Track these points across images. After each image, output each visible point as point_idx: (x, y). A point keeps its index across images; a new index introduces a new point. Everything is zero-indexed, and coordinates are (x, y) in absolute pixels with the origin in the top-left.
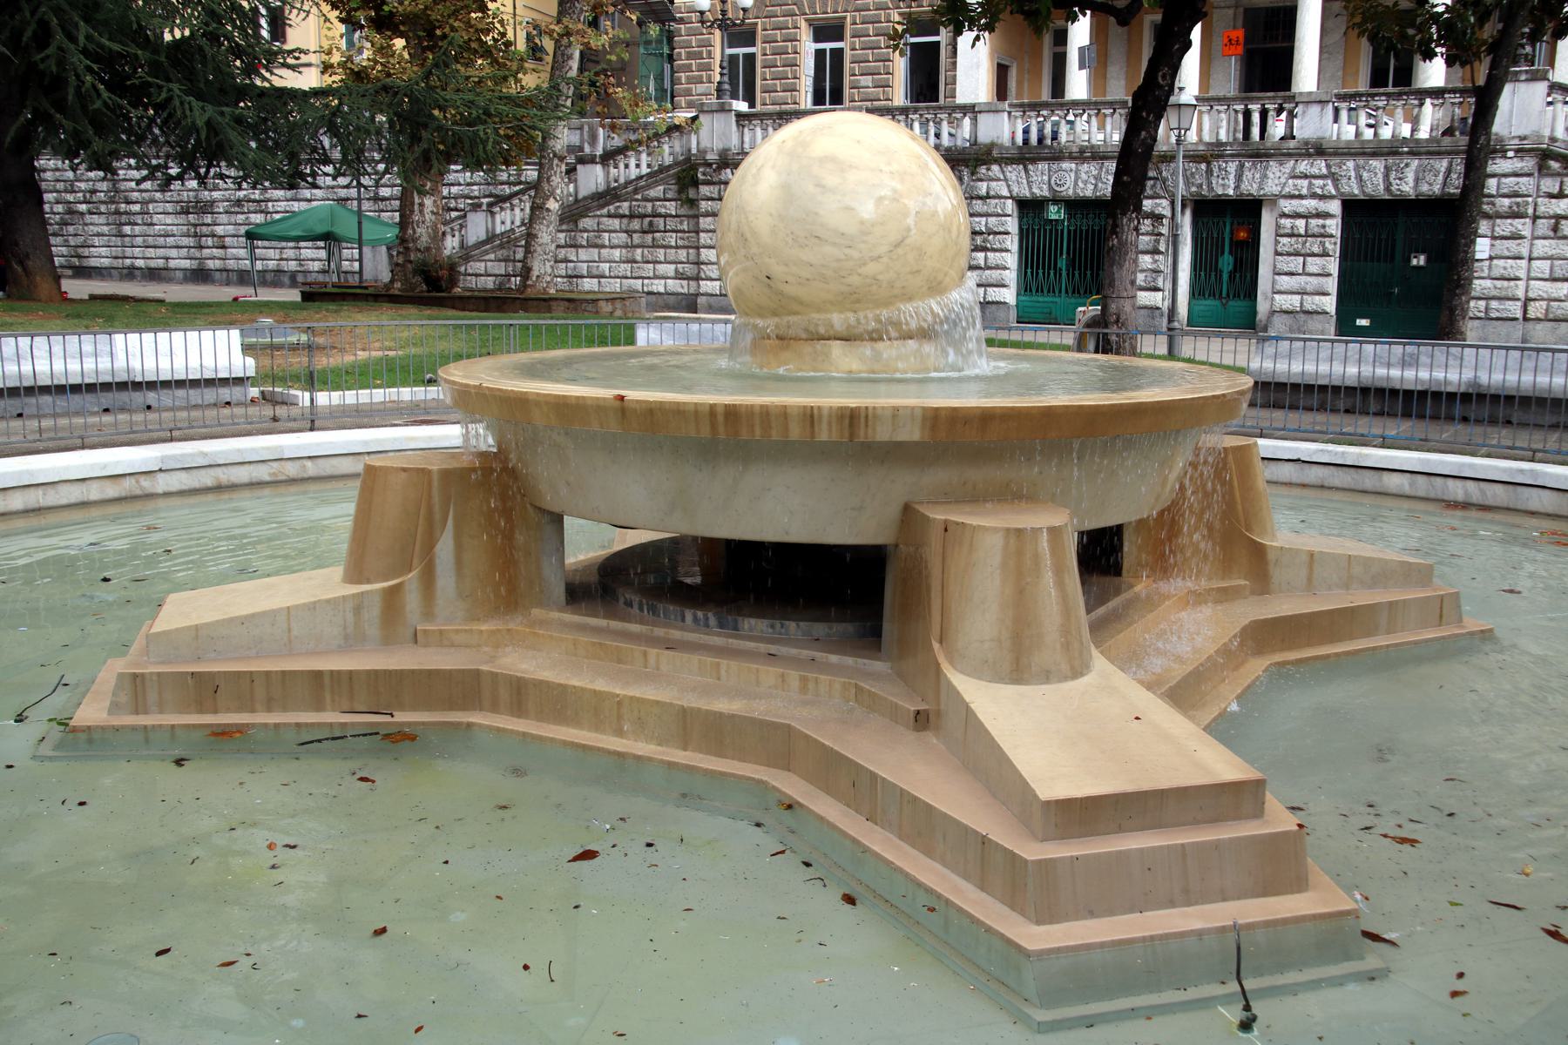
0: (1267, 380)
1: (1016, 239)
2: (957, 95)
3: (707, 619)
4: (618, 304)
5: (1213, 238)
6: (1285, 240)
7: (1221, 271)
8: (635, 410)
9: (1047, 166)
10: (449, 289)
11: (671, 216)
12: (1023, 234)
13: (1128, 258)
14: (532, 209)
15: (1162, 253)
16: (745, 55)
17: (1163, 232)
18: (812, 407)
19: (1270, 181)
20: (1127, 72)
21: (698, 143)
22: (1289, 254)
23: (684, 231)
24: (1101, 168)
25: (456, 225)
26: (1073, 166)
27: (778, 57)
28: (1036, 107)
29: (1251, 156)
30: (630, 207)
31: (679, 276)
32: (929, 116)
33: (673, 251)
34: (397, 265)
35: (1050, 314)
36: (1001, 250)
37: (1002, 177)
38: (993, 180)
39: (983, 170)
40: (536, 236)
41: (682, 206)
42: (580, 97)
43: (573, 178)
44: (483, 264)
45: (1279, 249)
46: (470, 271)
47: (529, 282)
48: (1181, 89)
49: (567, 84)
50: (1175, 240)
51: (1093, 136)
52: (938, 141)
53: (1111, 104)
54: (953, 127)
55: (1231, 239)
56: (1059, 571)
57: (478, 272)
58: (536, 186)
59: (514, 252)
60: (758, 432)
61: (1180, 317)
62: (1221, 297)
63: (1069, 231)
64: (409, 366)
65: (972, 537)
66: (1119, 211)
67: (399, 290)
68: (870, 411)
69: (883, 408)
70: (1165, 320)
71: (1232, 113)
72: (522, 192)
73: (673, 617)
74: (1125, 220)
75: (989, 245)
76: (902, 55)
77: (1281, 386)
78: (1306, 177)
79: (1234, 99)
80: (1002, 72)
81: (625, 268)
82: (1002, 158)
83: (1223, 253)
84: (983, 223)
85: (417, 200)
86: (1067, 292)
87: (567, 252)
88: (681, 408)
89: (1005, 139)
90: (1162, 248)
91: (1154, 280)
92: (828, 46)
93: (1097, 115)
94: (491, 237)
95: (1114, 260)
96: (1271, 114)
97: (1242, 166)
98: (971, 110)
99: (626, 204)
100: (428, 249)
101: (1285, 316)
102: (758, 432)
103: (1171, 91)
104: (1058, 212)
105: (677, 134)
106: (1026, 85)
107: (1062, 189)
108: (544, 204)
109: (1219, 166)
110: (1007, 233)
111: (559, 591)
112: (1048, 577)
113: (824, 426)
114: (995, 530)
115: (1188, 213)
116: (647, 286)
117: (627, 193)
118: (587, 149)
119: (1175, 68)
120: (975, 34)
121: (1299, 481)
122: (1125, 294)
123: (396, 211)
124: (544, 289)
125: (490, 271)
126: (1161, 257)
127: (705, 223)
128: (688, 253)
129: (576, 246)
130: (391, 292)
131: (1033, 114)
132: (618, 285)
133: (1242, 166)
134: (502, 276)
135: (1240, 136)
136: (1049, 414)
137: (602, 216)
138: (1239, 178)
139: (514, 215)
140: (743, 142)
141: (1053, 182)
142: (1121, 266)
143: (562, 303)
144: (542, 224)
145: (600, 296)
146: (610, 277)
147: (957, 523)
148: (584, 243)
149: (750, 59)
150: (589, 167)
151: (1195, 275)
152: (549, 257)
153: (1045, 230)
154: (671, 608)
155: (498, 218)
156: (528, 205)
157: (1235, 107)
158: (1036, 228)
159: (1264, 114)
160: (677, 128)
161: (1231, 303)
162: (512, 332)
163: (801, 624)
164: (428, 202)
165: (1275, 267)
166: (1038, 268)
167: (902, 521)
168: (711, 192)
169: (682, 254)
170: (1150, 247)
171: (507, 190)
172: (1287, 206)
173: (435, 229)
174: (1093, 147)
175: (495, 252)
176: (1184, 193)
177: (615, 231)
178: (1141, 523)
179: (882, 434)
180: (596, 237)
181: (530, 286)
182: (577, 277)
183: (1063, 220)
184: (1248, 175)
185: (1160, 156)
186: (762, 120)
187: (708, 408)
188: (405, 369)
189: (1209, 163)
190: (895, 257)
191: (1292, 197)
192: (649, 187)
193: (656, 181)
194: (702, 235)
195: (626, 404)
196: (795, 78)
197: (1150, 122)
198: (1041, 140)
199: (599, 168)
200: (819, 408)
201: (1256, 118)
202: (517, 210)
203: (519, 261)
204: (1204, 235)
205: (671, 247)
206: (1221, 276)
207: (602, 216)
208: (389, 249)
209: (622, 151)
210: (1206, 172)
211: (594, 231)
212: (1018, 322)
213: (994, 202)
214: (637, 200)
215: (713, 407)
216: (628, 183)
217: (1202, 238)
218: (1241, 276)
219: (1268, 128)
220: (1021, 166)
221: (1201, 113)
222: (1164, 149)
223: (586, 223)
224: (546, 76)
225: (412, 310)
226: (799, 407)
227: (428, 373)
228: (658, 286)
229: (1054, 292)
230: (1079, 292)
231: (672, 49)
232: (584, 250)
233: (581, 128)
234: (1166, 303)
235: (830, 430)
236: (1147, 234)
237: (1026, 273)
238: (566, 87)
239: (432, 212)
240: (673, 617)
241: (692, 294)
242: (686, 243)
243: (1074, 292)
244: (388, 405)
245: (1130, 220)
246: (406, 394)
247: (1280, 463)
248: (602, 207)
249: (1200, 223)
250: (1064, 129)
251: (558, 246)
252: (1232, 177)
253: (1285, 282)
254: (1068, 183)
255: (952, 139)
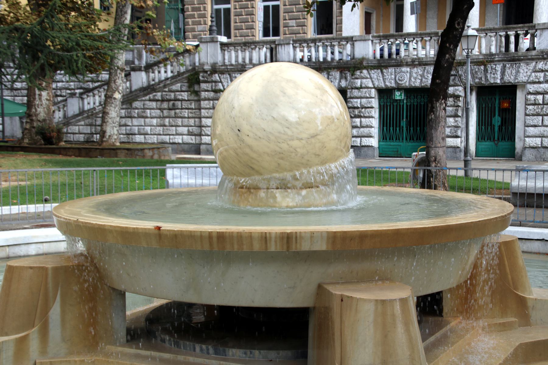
0: (522, 192)
1: (377, 111)
2: (343, 29)
3: (208, 349)
4: (156, 151)
5: (488, 107)
6: (531, 107)
7: (494, 126)
8: (167, 235)
9: (393, 70)
10: (57, 144)
11: (185, 100)
12: (382, 108)
13: (440, 125)
14: (105, 96)
15: (460, 116)
16: (225, 9)
17: (460, 105)
18: (266, 233)
19: (521, 74)
20: (438, 14)
21: (199, 60)
22: (533, 115)
23: (192, 109)
24: (424, 70)
25: (61, 105)
26: (408, 69)
27: (243, 10)
28: (387, 37)
29: (510, 61)
30: (162, 95)
31: (190, 134)
32: (327, 44)
33: (186, 120)
34: (26, 129)
35: (397, 151)
36: (369, 117)
37: (369, 76)
38: (363, 78)
39: (358, 73)
40: (108, 113)
41: (191, 95)
42: (132, 36)
43: (129, 79)
44: (77, 127)
45: (528, 113)
46: (70, 131)
47: (105, 139)
48: (468, 27)
49: (124, 28)
50: (467, 110)
51: (419, 52)
52: (333, 56)
53: (429, 34)
54: (341, 48)
55: (499, 108)
56: (407, 324)
57: (74, 132)
58: (108, 83)
59: (96, 121)
60: (236, 247)
61: (471, 152)
62: (494, 140)
63: (407, 106)
64: (34, 191)
65: (357, 305)
66: (434, 100)
67: (27, 144)
68: (298, 235)
69: (305, 232)
70: (462, 154)
71: (499, 37)
72: (100, 87)
73: (188, 348)
74: (438, 104)
75: (362, 115)
76: (311, 16)
77: (531, 195)
78: (542, 71)
79: (500, 29)
80: (368, 16)
81: (160, 130)
82: (368, 66)
83: (495, 116)
84: (359, 102)
85: (37, 92)
86: (406, 139)
87: (126, 121)
88: (193, 234)
89: (370, 56)
90: (460, 114)
91: (456, 132)
92: (271, 4)
93: (421, 41)
94: (82, 112)
95: (432, 126)
96: (521, 36)
97: (504, 67)
98: (350, 40)
99: (159, 94)
100: (44, 120)
101: (532, 150)
102: (236, 247)
103: (463, 29)
104: (401, 95)
105: (188, 54)
106: (381, 23)
107: (403, 82)
108: (113, 95)
109: (491, 67)
110: (372, 108)
111: (122, 334)
112: (400, 329)
113: (273, 243)
114: (370, 301)
115: (474, 94)
116: (172, 139)
117: (160, 88)
118: (137, 62)
119: (465, 18)
120: (352, 3)
121: (544, 252)
122: (439, 145)
123: (24, 96)
124: (113, 143)
125: (81, 131)
126: (459, 119)
127: (204, 104)
128: (195, 121)
129: (131, 117)
130: (23, 145)
131: (385, 41)
132: (156, 139)
133: (504, 67)
134: (88, 134)
135: (503, 49)
136: (397, 233)
137: (146, 100)
138: (503, 73)
139: (95, 99)
140: (224, 59)
141: (397, 79)
142: (436, 130)
143: (124, 151)
144: (111, 106)
145: (145, 146)
146: (151, 134)
147: (348, 297)
148: (136, 115)
149: (227, 11)
150: (138, 73)
151: (479, 128)
152: (116, 125)
153: (393, 106)
154: (188, 343)
155: (86, 102)
156: (103, 95)
157: (500, 33)
158: (388, 104)
159: (517, 37)
160: (187, 51)
161: (500, 143)
162: (95, 174)
163: (262, 351)
164: (44, 93)
165: (525, 122)
166: (390, 126)
167: (317, 294)
168: (207, 87)
169: (192, 122)
170: (453, 114)
171: (91, 85)
172: (531, 88)
173: (49, 109)
174: (419, 58)
175: (84, 121)
176: (472, 83)
177: (153, 109)
178: (450, 290)
179: (305, 247)
180: (143, 112)
181: (105, 141)
182: (132, 134)
183: (404, 100)
184: (508, 71)
185: (457, 63)
186: (235, 47)
187: (207, 234)
188: (31, 193)
189: (485, 66)
190: (309, 142)
191: (534, 83)
192: (172, 84)
193: (176, 81)
194: (203, 111)
195: (161, 232)
196: (253, 22)
197: (451, 49)
198: (390, 55)
199: (143, 74)
200: (270, 233)
201: (512, 39)
202: (97, 97)
203: (99, 126)
204: (484, 106)
205: (185, 118)
206: (494, 128)
207: (146, 100)
208: (21, 118)
209: (157, 64)
210: (484, 71)
211: (141, 109)
212: (380, 157)
213: (364, 90)
214: (165, 91)
215: (210, 233)
216: (160, 82)
217: (482, 108)
218: (505, 128)
219: (520, 44)
220: (379, 71)
221: (480, 37)
222: (460, 58)
223: (136, 104)
224: (112, 22)
225: (35, 157)
226: (259, 233)
227: (45, 195)
228: (178, 139)
229: (399, 139)
230: (413, 139)
231: (184, 5)
232: (136, 119)
233: (132, 51)
234: (463, 144)
235: (276, 245)
236: (451, 106)
237: (383, 129)
238: (124, 30)
239: (47, 99)
240: (188, 348)
241: (198, 144)
242: (194, 115)
243: (410, 139)
244: (21, 215)
245: (441, 104)
246: (32, 208)
247: (532, 241)
248: (146, 95)
249: (481, 99)
250: (403, 48)
251: (121, 117)
252: (499, 73)
253: (531, 131)
254: (406, 79)
255: (341, 55)
